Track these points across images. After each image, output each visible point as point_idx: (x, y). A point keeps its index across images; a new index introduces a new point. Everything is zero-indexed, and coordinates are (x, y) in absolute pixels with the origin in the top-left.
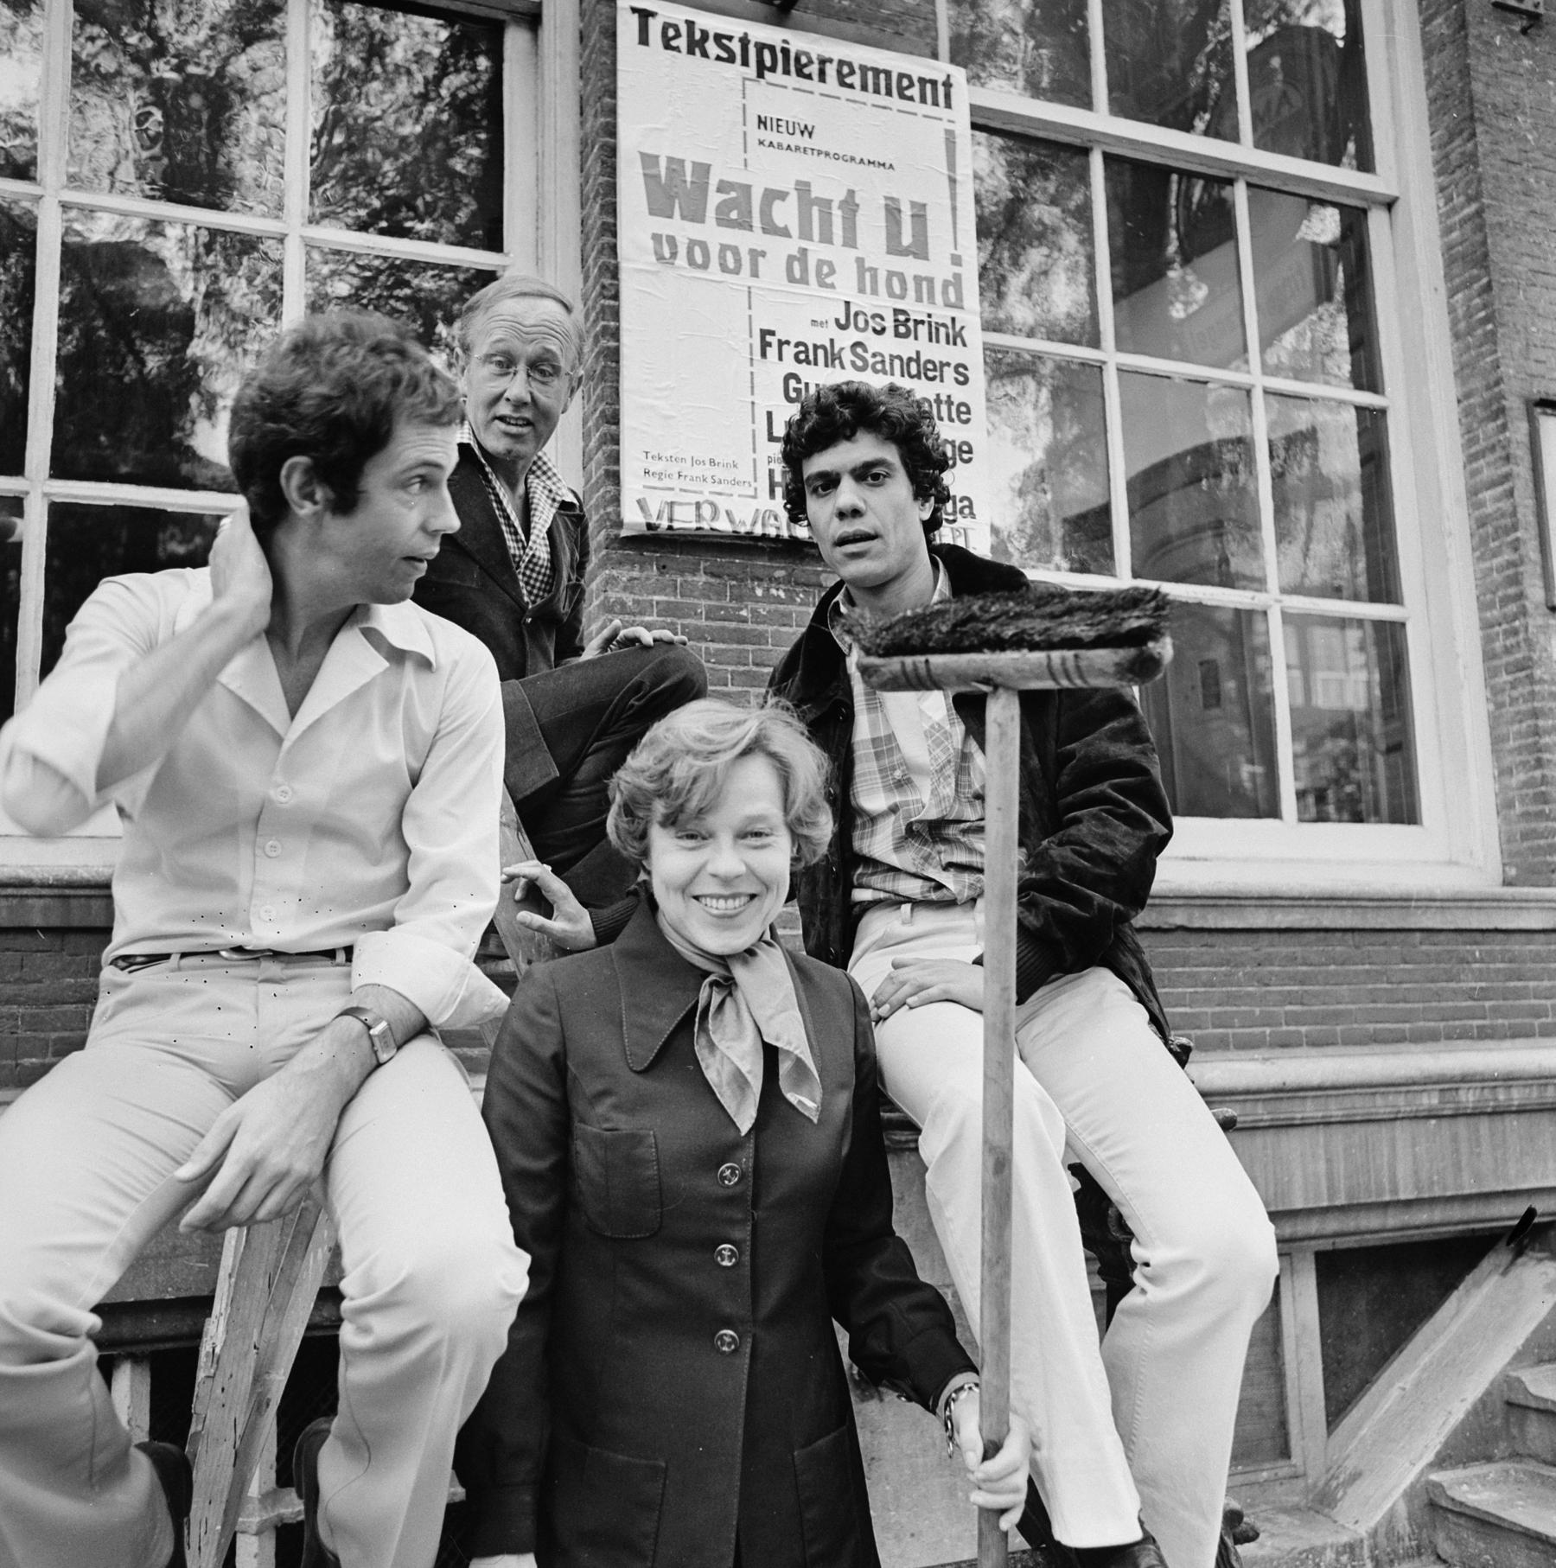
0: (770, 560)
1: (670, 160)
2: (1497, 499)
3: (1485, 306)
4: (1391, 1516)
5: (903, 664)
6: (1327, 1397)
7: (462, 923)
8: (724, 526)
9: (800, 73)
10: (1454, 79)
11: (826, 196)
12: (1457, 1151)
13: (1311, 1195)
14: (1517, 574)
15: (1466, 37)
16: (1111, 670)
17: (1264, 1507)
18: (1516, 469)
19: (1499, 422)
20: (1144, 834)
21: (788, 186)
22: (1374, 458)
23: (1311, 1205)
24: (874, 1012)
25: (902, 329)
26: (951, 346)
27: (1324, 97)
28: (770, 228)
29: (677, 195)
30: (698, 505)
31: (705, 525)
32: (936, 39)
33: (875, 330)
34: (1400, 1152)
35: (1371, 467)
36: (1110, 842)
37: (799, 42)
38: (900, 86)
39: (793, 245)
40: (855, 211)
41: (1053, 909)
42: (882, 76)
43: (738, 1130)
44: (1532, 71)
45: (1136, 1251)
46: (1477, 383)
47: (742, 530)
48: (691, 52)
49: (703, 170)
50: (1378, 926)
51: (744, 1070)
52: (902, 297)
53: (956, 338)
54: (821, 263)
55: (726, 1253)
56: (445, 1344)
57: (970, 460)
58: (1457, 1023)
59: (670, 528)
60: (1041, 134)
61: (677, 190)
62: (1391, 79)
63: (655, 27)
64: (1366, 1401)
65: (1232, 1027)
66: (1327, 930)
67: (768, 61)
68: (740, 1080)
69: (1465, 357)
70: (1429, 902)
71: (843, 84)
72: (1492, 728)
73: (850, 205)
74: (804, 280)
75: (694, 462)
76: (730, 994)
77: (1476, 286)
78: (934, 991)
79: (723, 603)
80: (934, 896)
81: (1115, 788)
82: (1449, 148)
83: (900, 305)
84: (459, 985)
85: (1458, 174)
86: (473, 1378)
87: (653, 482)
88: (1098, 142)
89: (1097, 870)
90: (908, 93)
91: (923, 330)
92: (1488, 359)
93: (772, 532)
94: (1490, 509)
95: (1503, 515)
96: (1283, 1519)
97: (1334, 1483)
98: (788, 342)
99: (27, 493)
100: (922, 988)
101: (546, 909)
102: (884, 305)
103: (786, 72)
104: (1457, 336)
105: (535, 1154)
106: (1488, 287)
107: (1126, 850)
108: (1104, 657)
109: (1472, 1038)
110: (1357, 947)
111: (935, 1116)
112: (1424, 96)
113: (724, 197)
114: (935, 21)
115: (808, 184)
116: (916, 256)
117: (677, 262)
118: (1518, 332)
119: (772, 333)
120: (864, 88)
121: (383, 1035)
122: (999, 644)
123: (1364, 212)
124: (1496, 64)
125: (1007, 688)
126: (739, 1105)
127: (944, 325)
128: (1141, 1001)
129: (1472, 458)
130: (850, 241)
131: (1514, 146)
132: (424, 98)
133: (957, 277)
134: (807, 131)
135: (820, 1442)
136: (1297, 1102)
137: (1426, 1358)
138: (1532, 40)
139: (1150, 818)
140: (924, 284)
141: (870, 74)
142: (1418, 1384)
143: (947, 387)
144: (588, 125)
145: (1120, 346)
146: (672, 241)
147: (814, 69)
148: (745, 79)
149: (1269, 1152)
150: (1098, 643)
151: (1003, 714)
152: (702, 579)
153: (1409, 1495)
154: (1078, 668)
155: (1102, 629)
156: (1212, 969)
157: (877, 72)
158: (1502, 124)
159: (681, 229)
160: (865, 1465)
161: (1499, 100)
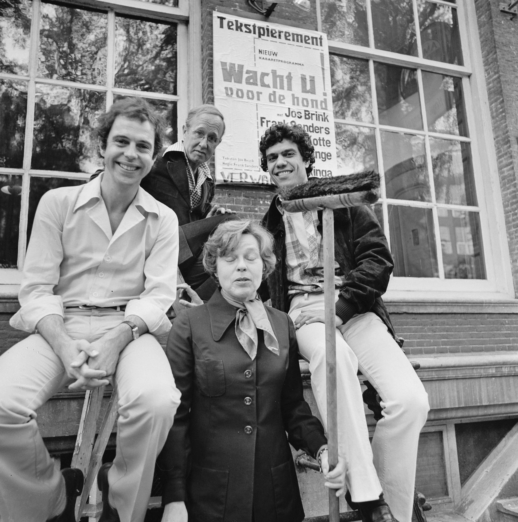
0: (265, 192)
1: (231, 64)
2: (508, 171)
3: (502, 107)
4: (484, 515)
5: (295, 202)
6: (461, 474)
7: (162, 301)
8: (249, 180)
9: (272, 36)
10: (489, 35)
11: (281, 74)
12: (502, 389)
13: (452, 403)
14: (516, 195)
15: (492, 21)
16: (360, 199)
17: (440, 512)
18: (514, 160)
19: (508, 145)
20: (384, 266)
21: (269, 71)
22: (467, 160)
23: (452, 407)
24: (295, 326)
25: (307, 117)
26: (324, 122)
27: (446, 43)
28: (263, 85)
29: (233, 75)
30: (241, 174)
31: (243, 180)
32: (317, 25)
33: (298, 117)
34: (483, 389)
35: (466, 162)
36: (372, 269)
37: (272, 26)
38: (305, 40)
39: (271, 90)
40: (291, 79)
41: (354, 292)
42: (299, 37)
43: (251, 359)
44: (514, 32)
45: (381, 404)
46: (500, 133)
47: (255, 182)
48: (237, 30)
49: (241, 67)
50: (473, 312)
51: (252, 338)
52: (307, 106)
53: (325, 119)
54: (280, 96)
55: (248, 400)
56: (153, 419)
57: (330, 159)
58: (501, 345)
59: (232, 181)
60: (353, 55)
61: (233, 73)
62: (468, 36)
63: (225, 22)
64: (474, 476)
65: (424, 346)
66: (455, 314)
67: (262, 33)
68: (251, 342)
69: (496, 125)
70: (489, 304)
71: (286, 39)
72: (510, 247)
73: (289, 77)
74: (275, 101)
75: (239, 160)
76: (246, 315)
77: (499, 101)
78: (314, 319)
79: (249, 206)
80: (315, 290)
81: (374, 252)
82: (488, 57)
83: (307, 109)
84: (160, 321)
85: (491, 65)
86: (162, 434)
87: (226, 166)
88: (372, 57)
89: (369, 279)
90: (308, 42)
91: (314, 117)
92: (504, 125)
93: (265, 182)
94: (506, 174)
95: (510, 176)
96: (447, 517)
97: (464, 505)
98: (270, 121)
99: (23, 174)
100: (310, 318)
101: (189, 299)
102: (302, 109)
103: (268, 36)
104: (493, 118)
105: (183, 371)
106: (503, 101)
107: (378, 272)
108: (357, 195)
109: (506, 350)
110: (466, 319)
111: (314, 357)
112: (479, 40)
113: (249, 75)
114: (316, 19)
115: (276, 71)
116: (312, 93)
117: (233, 96)
118: (513, 116)
119: (265, 118)
120: (294, 40)
121: (136, 332)
122: (324, 193)
123: (461, 78)
124: (503, 30)
125: (328, 208)
126: (250, 351)
127: (321, 115)
128: (385, 323)
129: (499, 157)
130: (290, 88)
131: (510, 55)
132: (155, 58)
133: (325, 100)
134: (275, 54)
135: (280, 466)
136: (446, 372)
137: (495, 461)
138: (514, 22)
139: (386, 261)
140: (314, 102)
141: (295, 36)
142: (492, 470)
143: (323, 135)
144: (204, 54)
145: (380, 123)
146: (231, 89)
147: (277, 35)
148: (255, 38)
149: (437, 389)
150: (355, 190)
151: (328, 218)
152: (242, 198)
153: (490, 508)
154: (349, 199)
155: (356, 185)
156: (416, 327)
157: (297, 35)
158: (505, 49)
159: (234, 85)
160: (301, 495)
161: (504, 41)
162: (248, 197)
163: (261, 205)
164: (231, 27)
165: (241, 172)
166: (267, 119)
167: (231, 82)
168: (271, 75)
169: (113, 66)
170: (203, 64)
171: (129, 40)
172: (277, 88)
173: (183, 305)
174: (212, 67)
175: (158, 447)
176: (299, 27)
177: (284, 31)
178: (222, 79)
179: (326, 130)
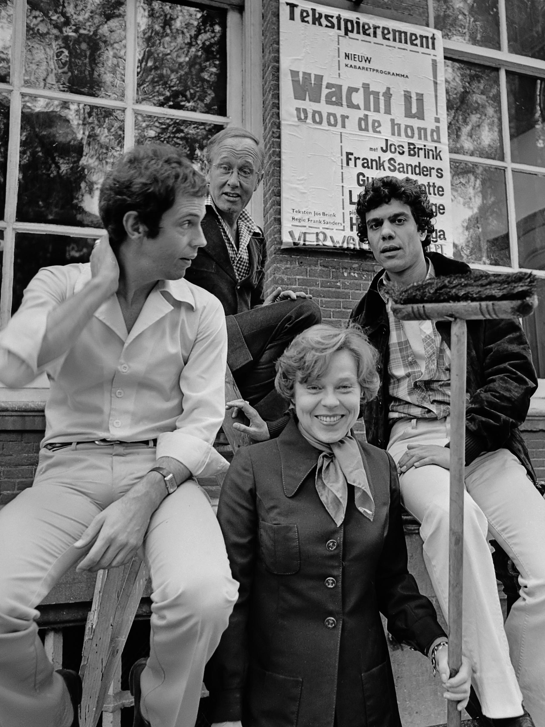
0: (351, 259)
5: (412, 308)
7: (208, 428)
8: (329, 243)
9: (364, 33)
16: (510, 310)
20: (525, 387)
21: (359, 85)
25: (412, 152)
26: (435, 160)
28: (350, 105)
30: (317, 234)
31: (320, 243)
32: (428, 17)
33: (399, 153)
36: (509, 390)
37: (364, 19)
38: (411, 39)
39: (361, 113)
41: (482, 421)
42: (403, 35)
47: (338, 245)
49: (319, 78)
52: (412, 137)
54: (374, 121)
56: (200, 624)
59: (304, 244)
61: (308, 87)
63: (297, 11)
67: (350, 28)
68: (337, 501)
73: (388, 94)
74: (366, 130)
75: (315, 214)
76: (332, 461)
80: (427, 416)
83: (411, 141)
84: (206, 457)
86: (213, 639)
87: (297, 223)
89: (503, 404)
90: (415, 42)
91: (422, 153)
93: (352, 246)
99: (6, 228)
100: (422, 458)
101: (247, 422)
102: (404, 140)
103: (358, 33)
107: (516, 394)
108: (507, 305)
111: (427, 518)
113: (330, 90)
114: (427, 9)
115: (368, 85)
116: (419, 118)
117: (308, 121)
119: (352, 154)
120: (395, 40)
122: (457, 298)
126: (336, 513)
128: (523, 464)
130: (388, 111)
133: (438, 128)
134: (368, 60)
135: (374, 669)
139: (527, 379)
140: (422, 131)
141: (397, 34)
143: (433, 179)
144: (266, 57)
145: (513, 161)
146: (305, 111)
147: (371, 31)
148: (339, 36)
151: (459, 331)
154: (494, 309)
155: (505, 292)
157: (400, 32)
159: (309, 106)
160: (395, 680)
162: (327, 267)
163: (345, 278)
164: (306, 19)
165: (318, 231)
166: (355, 155)
167: (305, 100)
168: (361, 91)
169: (134, 71)
170: (264, 72)
171: (152, 14)
172: (370, 111)
173: (238, 430)
174: (278, 77)
175: (207, 656)
176: (403, 21)
177: (381, 26)
178: (292, 95)
179: (437, 172)
